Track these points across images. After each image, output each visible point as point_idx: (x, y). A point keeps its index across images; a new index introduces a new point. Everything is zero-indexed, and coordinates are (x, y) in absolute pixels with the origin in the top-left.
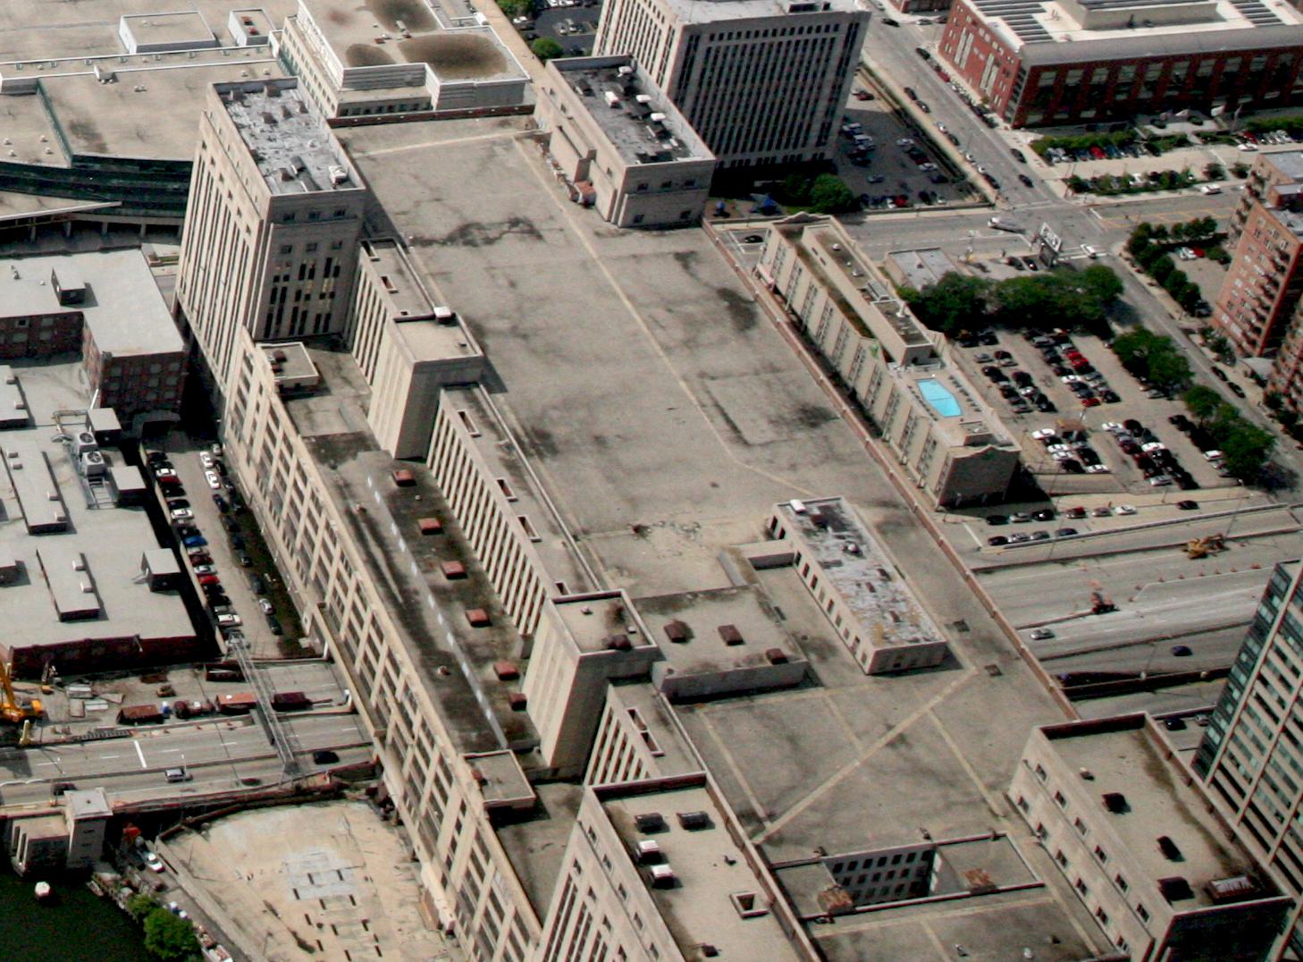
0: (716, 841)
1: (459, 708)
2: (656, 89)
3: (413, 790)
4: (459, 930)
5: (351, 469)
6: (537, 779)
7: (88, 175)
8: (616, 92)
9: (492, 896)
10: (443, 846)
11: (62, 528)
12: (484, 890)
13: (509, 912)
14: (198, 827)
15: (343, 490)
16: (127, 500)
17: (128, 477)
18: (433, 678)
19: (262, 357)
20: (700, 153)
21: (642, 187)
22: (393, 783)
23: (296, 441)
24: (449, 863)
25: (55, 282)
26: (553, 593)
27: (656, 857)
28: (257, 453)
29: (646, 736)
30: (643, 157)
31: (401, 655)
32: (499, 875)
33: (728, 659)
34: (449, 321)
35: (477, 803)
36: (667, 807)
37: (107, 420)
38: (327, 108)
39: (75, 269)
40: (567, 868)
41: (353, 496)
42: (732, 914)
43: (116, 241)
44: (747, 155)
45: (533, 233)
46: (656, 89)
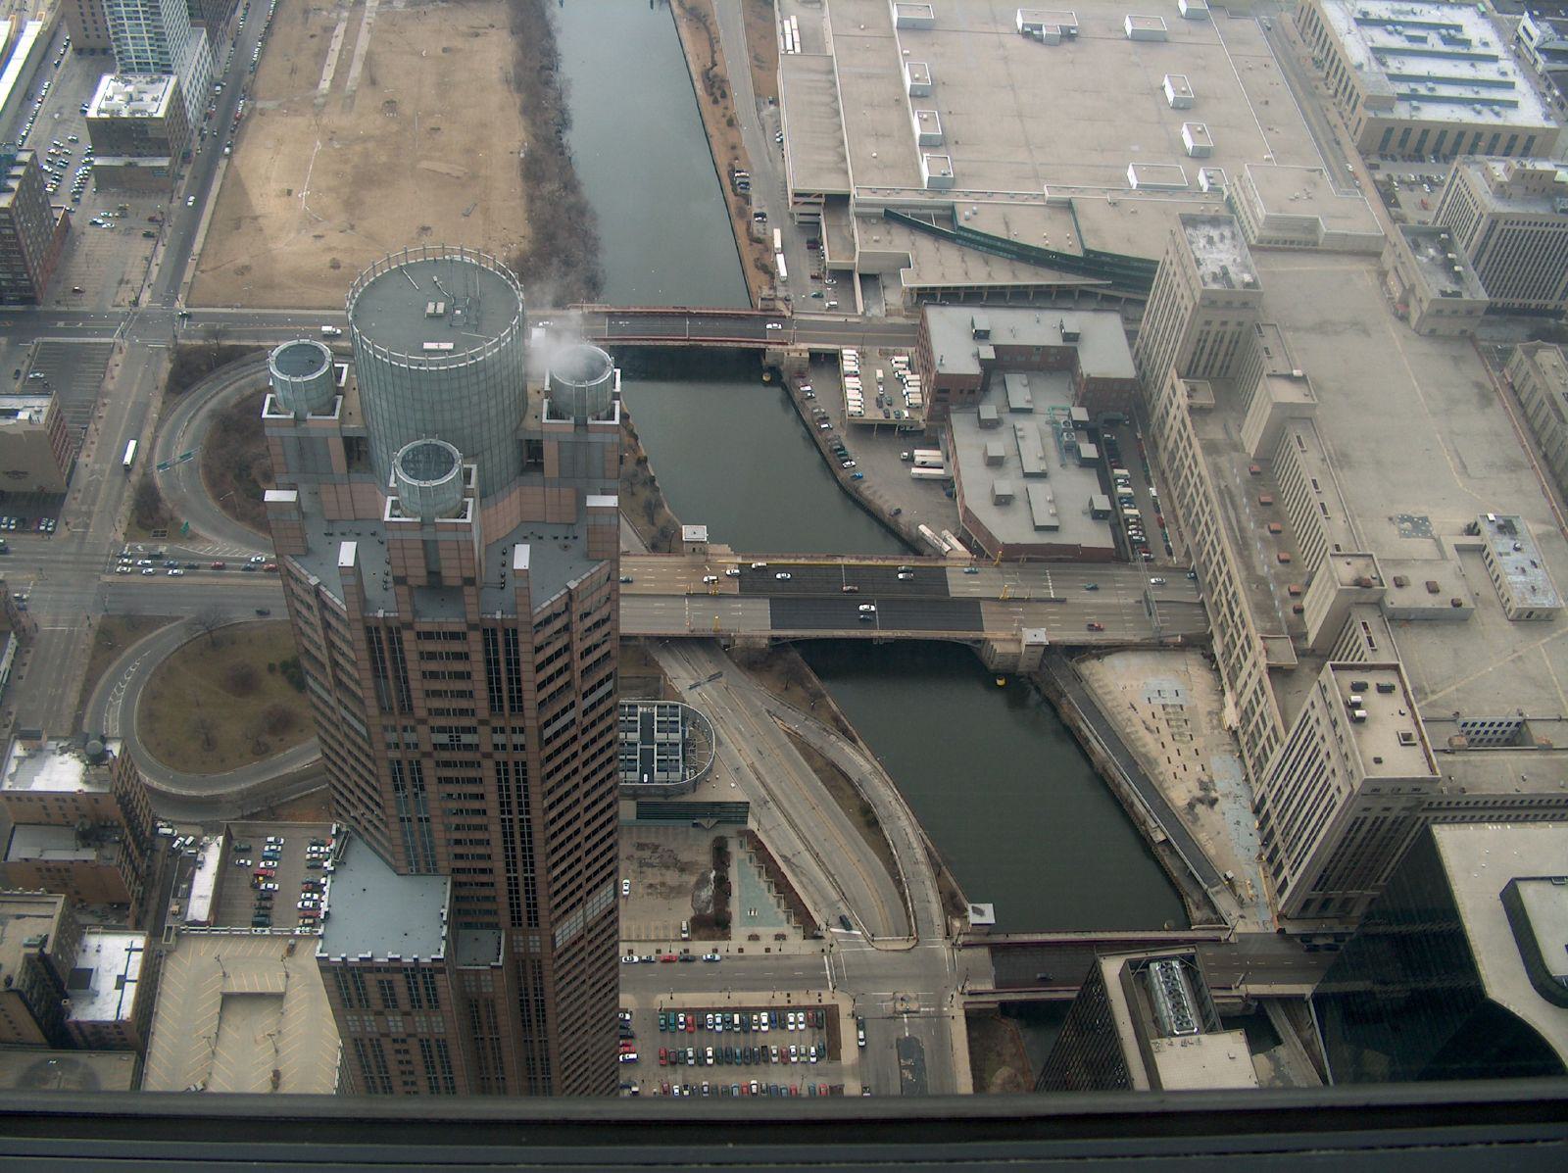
0: (1396, 701)
1: (1264, 609)
2: (1462, 254)
3: (1228, 650)
4: (1240, 732)
5: (1223, 461)
6: (1301, 654)
7: (1093, 263)
8: (1436, 249)
9: (1262, 714)
10: (1239, 684)
11: (1041, 476)
12: (1258, 711)
13: (1270, 725)
14: (1098, 657)
15: (1217, 472)
16: (1085, 463)
17: (1089, 450)
18: (1250, 589)
19: (1181, 387)
20: (1482, 296)
21: (1439, 312)
22: (1218, 648)
23: (1195, 442)
24: (1241, 694)
25: (1062, 327)
26: (1332, 550)
27: (1357, 705)
28: (1171, 445)
29: (1370, 639)
30: (1444, 293)
31: (1234, 571)
32: (1269, 705)
33: (1429, 602)
34: (1302, 380)
35: (1263, 662)
36: (1372, 680)
37: (1081, 414)
38: (1251, 237)
39: (1074, 321)
40: (1307, 705)
41: (1223, 478)
42: (1393, 742)
43: (1105, 305)
44: (1514, 300)
45: (1366, 332)
46: (1462, 254)
